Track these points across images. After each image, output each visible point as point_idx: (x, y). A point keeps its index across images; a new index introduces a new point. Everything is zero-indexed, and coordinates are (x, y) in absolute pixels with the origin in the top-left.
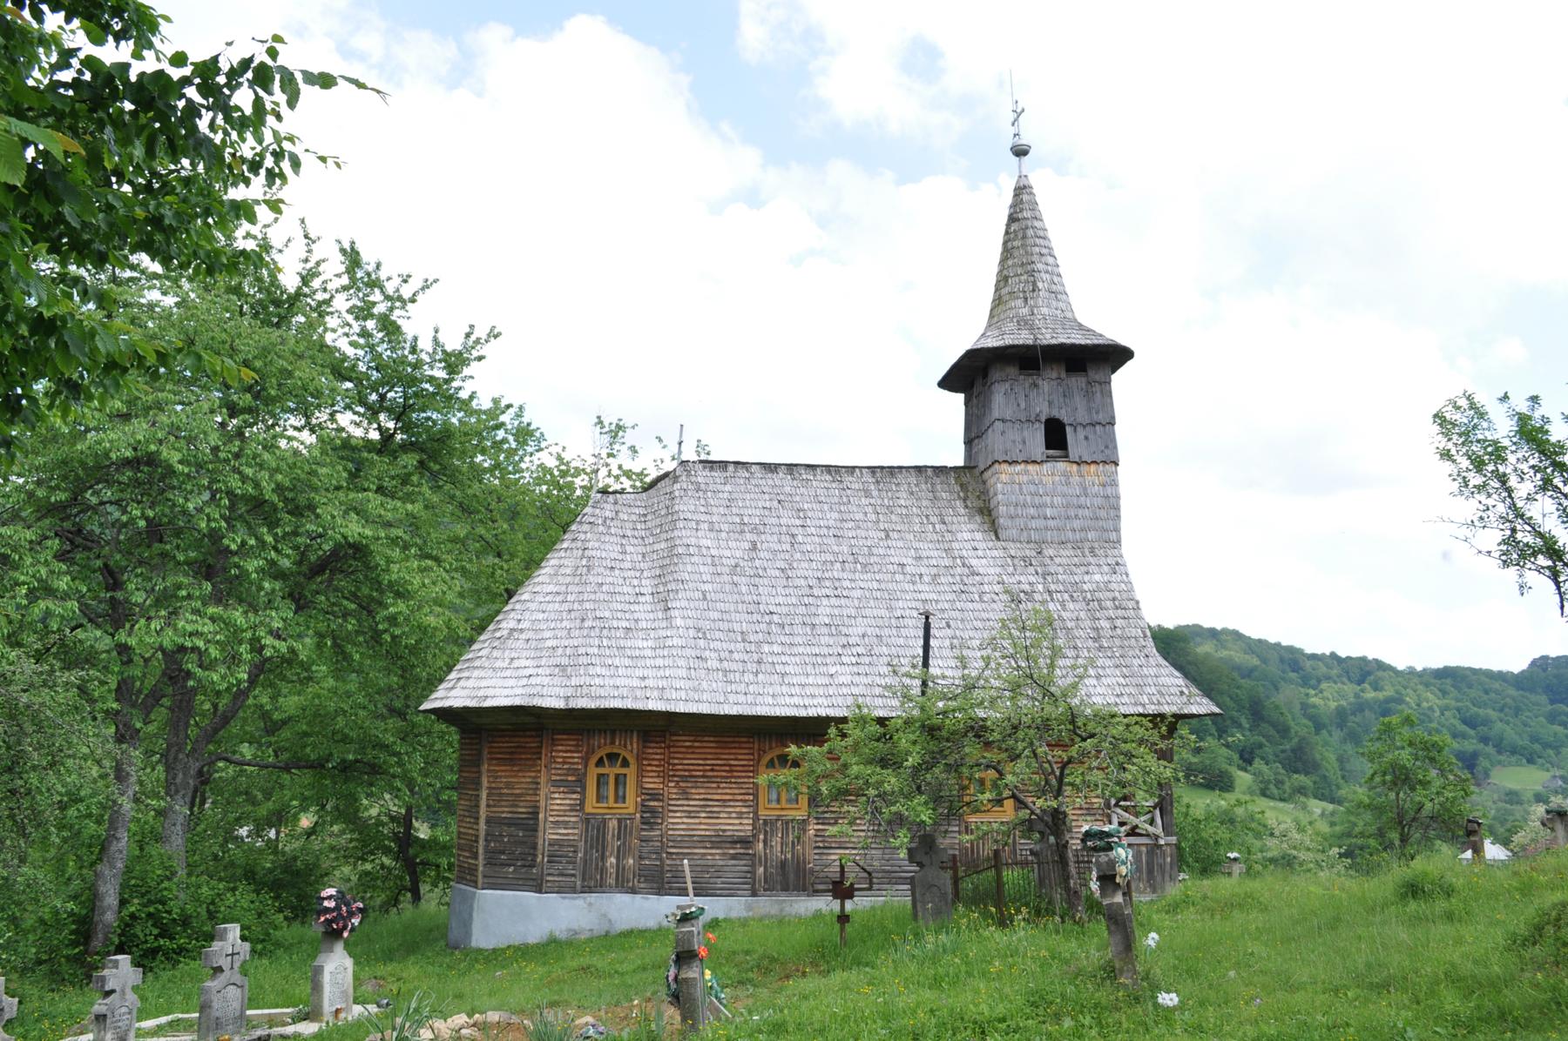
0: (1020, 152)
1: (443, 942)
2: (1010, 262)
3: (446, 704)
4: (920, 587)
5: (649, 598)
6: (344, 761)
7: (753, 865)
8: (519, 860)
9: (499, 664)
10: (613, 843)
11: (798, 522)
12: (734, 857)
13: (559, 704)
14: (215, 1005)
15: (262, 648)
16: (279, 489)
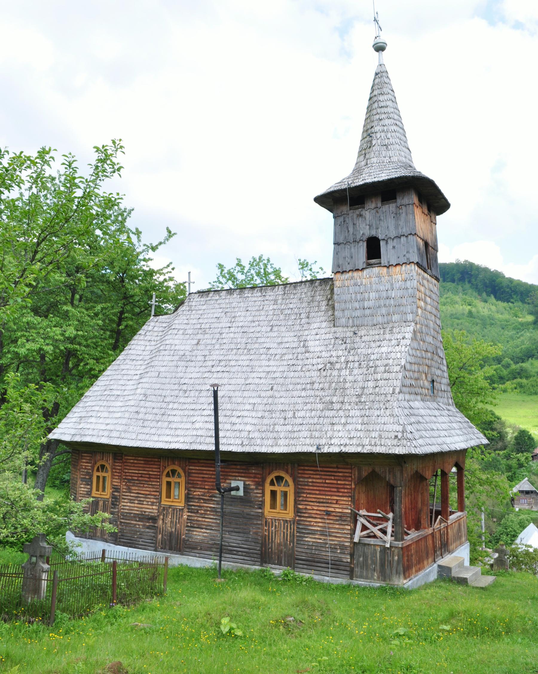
7: (156, 533)
12: (148, 527)
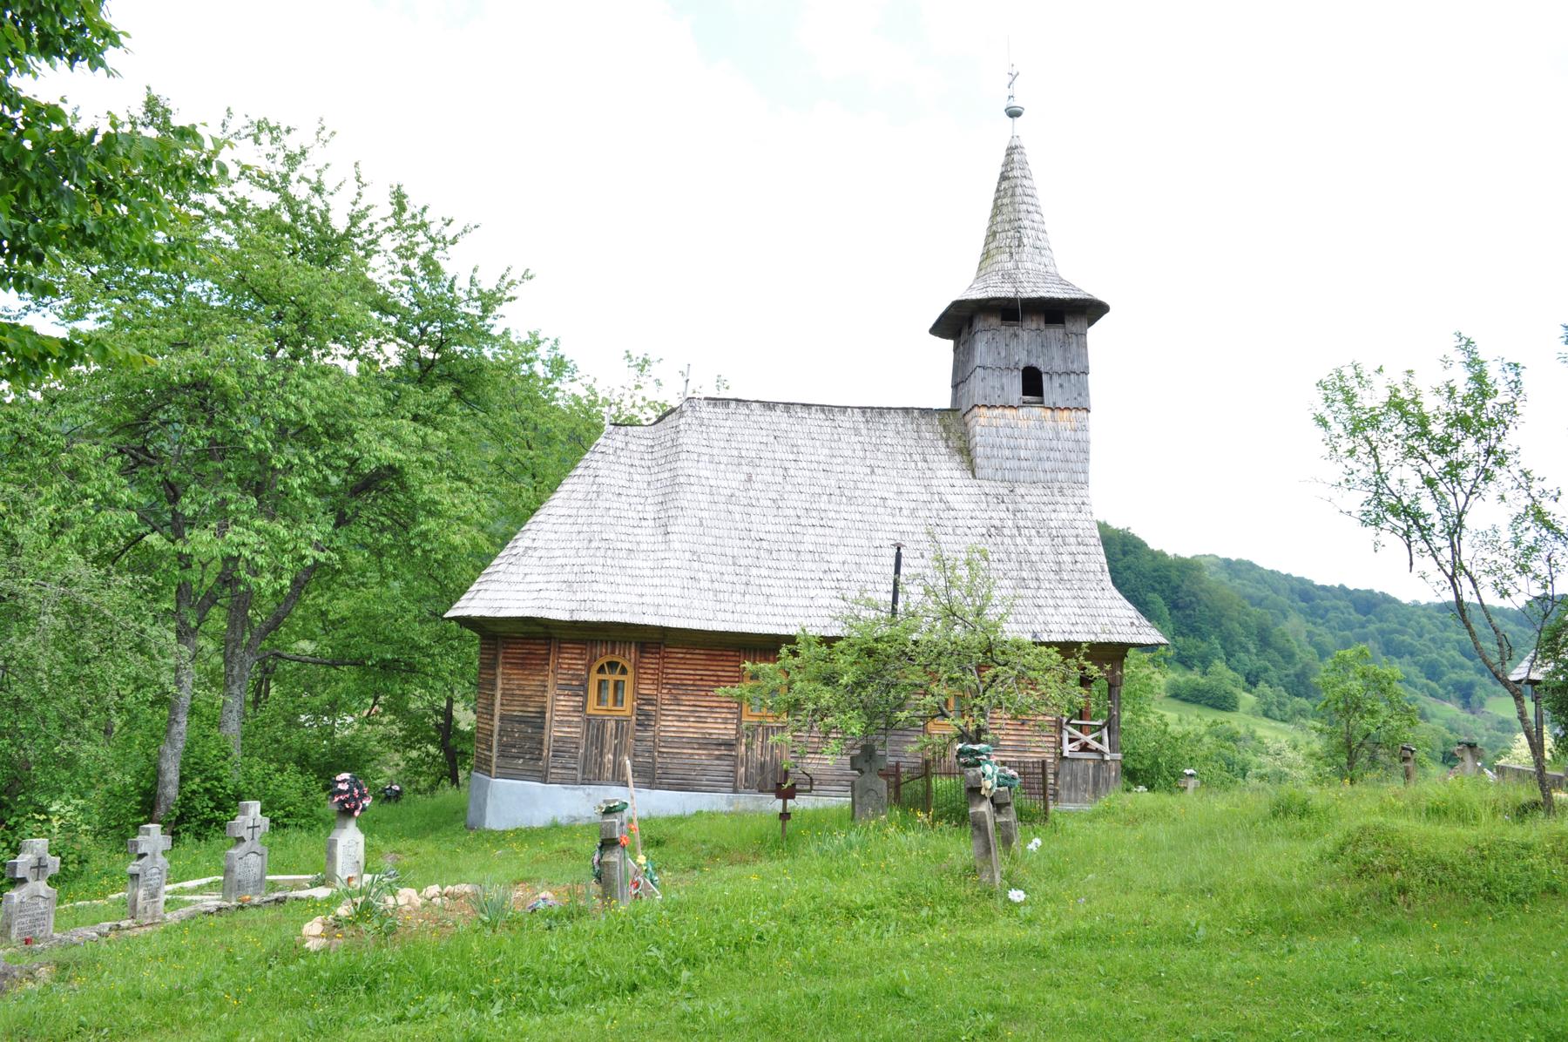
0: (1014, 114)
1: (460, 824)
2: (999, 219)
3: (465, 613)
4: (900, 520)
5: (651, 523)
6: (384, 660)
7: (735, 766)
8: (528, 753)
9: (514, 578)
10: (610, 742)
11: (792, 457)
12: (718, 758)
13: (565, 617)
14: (237, 870)
15: (304, 557)
16: (319, 415)
